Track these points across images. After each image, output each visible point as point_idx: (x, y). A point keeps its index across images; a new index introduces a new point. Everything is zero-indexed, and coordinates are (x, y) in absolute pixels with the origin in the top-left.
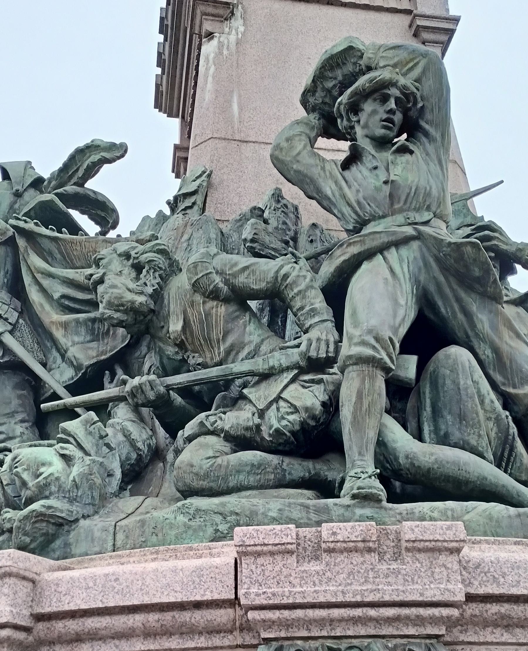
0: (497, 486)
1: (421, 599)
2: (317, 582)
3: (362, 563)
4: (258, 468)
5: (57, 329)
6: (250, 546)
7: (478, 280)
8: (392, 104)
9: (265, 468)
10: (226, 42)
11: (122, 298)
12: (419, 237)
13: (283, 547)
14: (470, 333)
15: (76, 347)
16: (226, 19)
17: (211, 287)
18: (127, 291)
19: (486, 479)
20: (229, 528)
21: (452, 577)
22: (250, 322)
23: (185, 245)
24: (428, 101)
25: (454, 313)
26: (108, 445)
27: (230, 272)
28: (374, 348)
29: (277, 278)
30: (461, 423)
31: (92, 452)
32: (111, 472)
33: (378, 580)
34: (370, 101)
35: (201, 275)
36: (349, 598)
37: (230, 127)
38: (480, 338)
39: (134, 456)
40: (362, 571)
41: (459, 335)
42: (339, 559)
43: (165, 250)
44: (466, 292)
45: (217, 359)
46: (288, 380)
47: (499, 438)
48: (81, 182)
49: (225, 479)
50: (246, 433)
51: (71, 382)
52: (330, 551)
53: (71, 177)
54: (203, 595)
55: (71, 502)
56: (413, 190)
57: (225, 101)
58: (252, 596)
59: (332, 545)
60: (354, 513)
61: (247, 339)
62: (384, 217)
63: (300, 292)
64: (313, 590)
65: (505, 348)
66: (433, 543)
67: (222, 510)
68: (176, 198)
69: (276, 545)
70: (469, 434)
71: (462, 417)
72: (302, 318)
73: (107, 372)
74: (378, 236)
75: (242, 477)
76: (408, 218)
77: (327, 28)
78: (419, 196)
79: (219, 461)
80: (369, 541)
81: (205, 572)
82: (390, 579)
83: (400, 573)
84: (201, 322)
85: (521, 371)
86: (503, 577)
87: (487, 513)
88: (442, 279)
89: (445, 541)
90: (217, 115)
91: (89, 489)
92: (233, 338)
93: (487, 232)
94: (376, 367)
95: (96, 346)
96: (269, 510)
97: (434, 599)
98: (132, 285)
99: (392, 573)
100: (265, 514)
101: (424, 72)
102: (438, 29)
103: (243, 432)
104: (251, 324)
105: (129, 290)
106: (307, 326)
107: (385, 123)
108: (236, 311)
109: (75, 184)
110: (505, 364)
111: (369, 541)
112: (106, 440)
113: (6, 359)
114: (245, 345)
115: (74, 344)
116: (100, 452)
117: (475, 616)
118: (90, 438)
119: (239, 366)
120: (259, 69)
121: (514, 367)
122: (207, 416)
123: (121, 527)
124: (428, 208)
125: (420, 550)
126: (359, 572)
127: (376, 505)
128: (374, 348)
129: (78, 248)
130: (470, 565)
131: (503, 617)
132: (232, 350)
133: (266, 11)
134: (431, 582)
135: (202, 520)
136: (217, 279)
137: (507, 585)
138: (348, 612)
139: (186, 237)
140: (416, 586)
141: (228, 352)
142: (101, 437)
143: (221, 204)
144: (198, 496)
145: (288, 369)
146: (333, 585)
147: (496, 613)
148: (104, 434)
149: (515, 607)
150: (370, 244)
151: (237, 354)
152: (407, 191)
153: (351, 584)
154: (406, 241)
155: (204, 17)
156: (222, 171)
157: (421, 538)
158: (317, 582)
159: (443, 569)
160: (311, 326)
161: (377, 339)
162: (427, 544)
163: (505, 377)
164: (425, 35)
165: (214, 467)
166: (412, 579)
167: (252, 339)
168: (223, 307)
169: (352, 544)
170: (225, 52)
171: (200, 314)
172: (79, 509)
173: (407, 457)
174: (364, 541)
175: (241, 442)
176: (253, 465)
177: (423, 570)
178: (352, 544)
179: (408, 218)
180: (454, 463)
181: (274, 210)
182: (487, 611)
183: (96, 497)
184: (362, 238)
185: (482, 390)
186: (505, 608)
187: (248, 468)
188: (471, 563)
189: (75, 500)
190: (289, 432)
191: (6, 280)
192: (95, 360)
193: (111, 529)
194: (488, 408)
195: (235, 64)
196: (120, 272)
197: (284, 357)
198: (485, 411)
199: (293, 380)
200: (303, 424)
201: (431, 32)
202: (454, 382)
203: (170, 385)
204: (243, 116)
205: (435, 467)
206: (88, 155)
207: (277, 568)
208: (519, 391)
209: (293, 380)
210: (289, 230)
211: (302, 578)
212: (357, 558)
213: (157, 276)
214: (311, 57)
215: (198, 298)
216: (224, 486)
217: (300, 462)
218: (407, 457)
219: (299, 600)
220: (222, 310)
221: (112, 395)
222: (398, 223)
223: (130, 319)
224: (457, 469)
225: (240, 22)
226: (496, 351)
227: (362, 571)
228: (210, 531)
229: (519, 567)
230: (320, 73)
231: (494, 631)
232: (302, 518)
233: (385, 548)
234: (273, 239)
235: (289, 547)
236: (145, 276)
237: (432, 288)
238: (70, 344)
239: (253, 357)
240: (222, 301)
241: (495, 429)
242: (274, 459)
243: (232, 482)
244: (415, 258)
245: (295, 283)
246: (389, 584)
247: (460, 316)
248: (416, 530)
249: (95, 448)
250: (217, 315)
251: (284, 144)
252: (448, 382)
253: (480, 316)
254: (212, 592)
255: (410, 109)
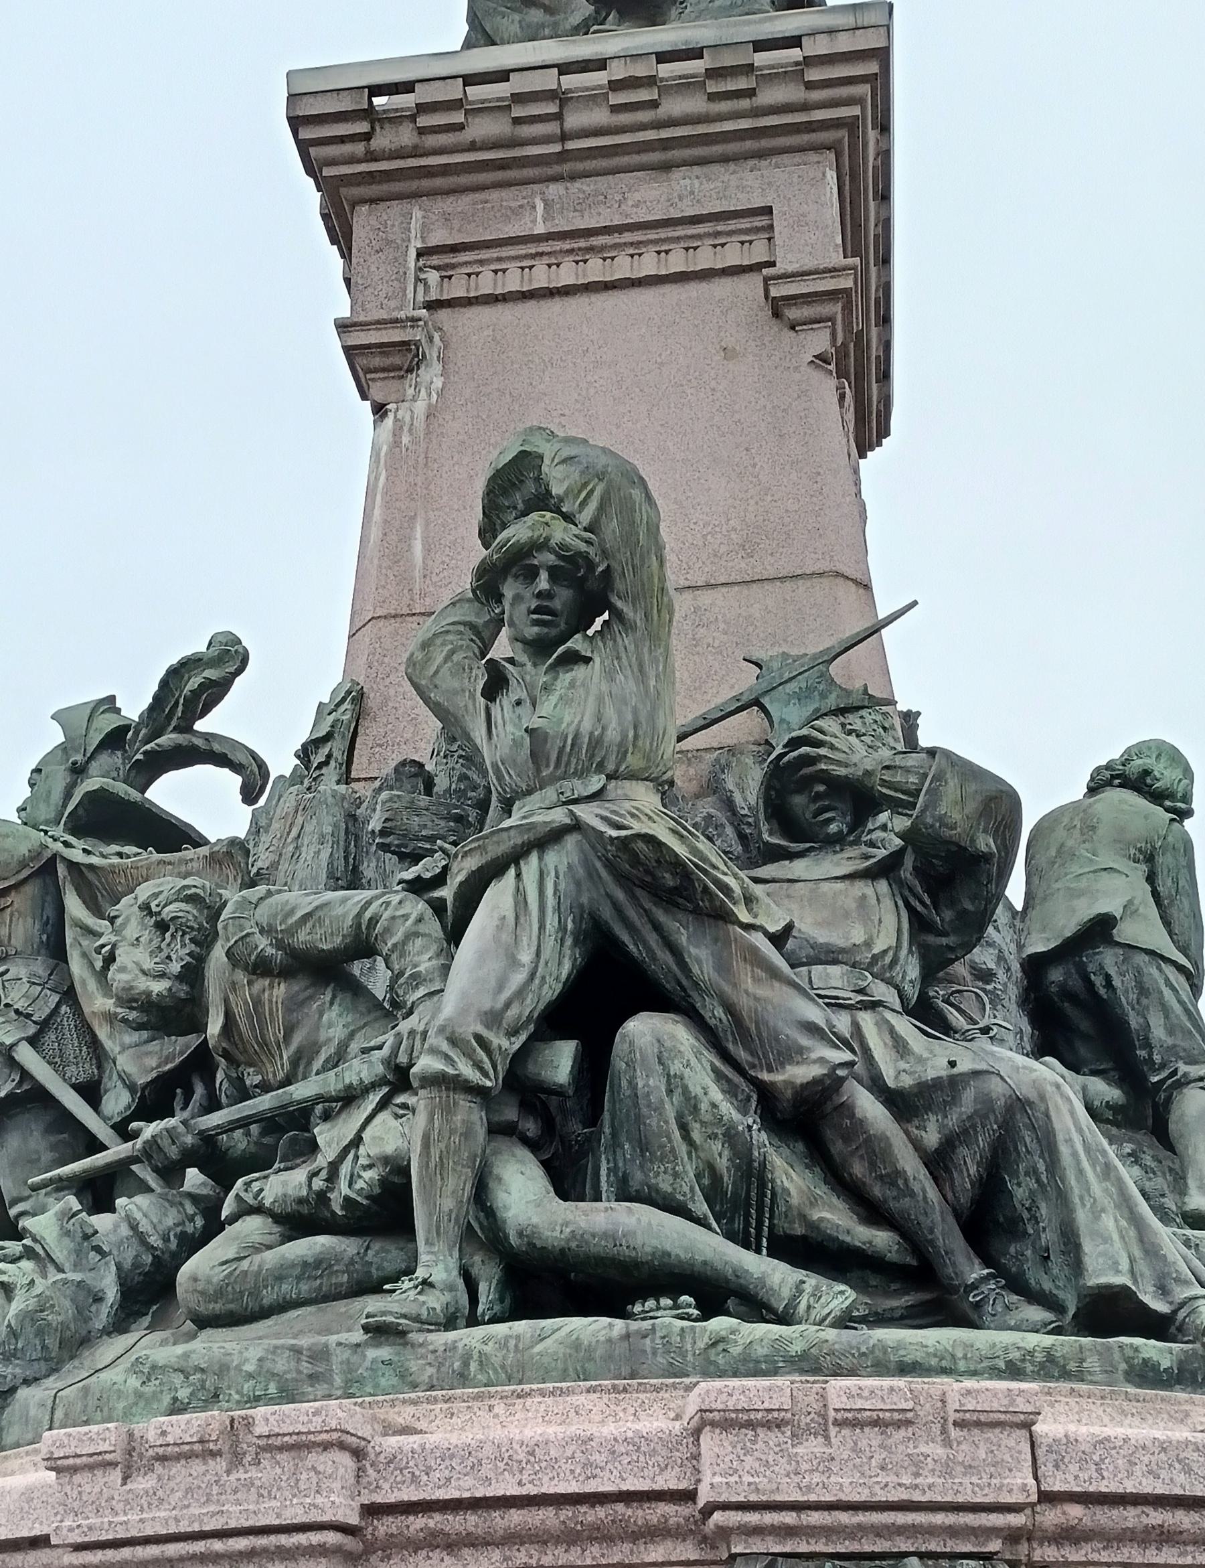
0: (693, 1265)
1: (277, 1522)
2: (145, 1506)
3: (204, 1474)
4: (317, 1267)
5: (100, 1025)
6: (60, 1458)
7: (676, 891)
8: (543, 583)
9: (331, 1266)
10: (407, 419)
11: (131, 988)
12: (576, 826)
13: (100, 1458)
14: (685, 982)
15: (128, 1052)
16: (410, 370)
17: (253, 957)
18: (140, 975)
19: (669, 1255)
20: (191, 1394)
21: (324, 1486)
22: (332, 1004)
23: (291, 848)
24: (614, 557)
25: (649, 950)
26: (98, 1249)
27: (283, 927)
28: (447, 1057)
29: (360, 924)
30: (643, 1156)
31: (67, 1267)
32: (100, 1294)
33: (223, 1497)
34: (510, 580)
35: (232, 942)
36: (184, 1527)
37: (405, 591)
38: (701, 989)
39: (148, 1259)
40: (204, 1486)
41: (668, 986)
42: (174, 1471)
43: (197, 895)
44: (666, 911)
45: (281, 1075)
46: (373, 1106)
47: (738, 1168)
48: (183, 724)
49: (255, 1293)
50: (300, 1208)
51: (128, 1113)
52: (163, 1459)
53: (169, 717)
54: (31, 1529)
55: (8, 1360)
56: (569, 741)
57: (400, 541)
58: (65, 1531)
59: (161, 1451)
60: (365, 1356)
61: (323, 1035)
62: (529, 792)
63: (395, 945)
64: (138, 1518)
65: (744, 1003)
66: (295, 1437)
67: (185, 1364)
68: (305, 747)
69: (91, 1455)
70: (657, 1174)
71: (643, 1146)
72: (401, 992)
73: (178, 1091)
74: (505, 835)
75: (285, 1287)
76: (562, 793)
77: (601, 342)
78: (580, 748)
79: (245, 1265)
80: (208, 1441)
81: (35, 1495)
82: (239, 1495)
83: (253, 1484)
84: (249, 1016)
85: (777, 1040)
86: (427, 1474)
87: (574, 1337)
88: (620, 895)
89: (310, 1433)
90: (384, 571)
91: (36, 1336)
92: (300, 1039)
93: (804, 750)
94: (454, 1089)
95: (158, 1048)
96: (247, 1360)
97: (295, 1521)
98: (148, 964)
99: (243, 1486)
100: (238, 1368)
101: (601, 508)
102: (816, 294)
103: (295, 1207)
104: (335, 1007)
105: (144, 972)
106: (409, 1004)
107: (535, 616)
108: (306, 988)
109: (175, 729)
110: (748, 1030)
111: (208, 1441)
112: (95, 1241)
113: (26, 1087)
114: (321, 1047)
115: (124, 1048)
116: (84, 1261)
117: (392, 1535)
118: (66, 1241)
119: (301, 1091)
120: (466, 460)
121: (765, 1035)
122: (248, 1184)
123: (62, 1397)
124: (600, 768)
125: (281, 1449)
126: (199, 1487)
127: (399, 1341)
128: (447, 1057)
129: (123, 881)
130: (382, 1458)
131: (434, 1534)
132: (299, 1059)
133: (486, 333)
134: (294, 1496)
135: (157, 1382)
136: (263, 943)
137: (432, 1485)
138: (187, 1548)
139: (294, 833)
140: (274, 1503)
141: (295, 1062)
142: (86, 1237)
143: (381, 746)
144: (211, 1327)
145: (373, 1086)
146: (165, 1510)
147: (422, 1529)
148: (90, 1231)
149: (450, 1518)
150: (497, 849)
151: (309, 1063)
152: (559, 743)
153: (188, 1506)
154: (554, 836)
155: (368, 376)
156: (387, 681)
157: (277, 1430)
158: (145, 1506)
159: (312, 1474)
160: (413, 1003)
161: (453, 1041)
162: (286, 1439)
163: (753, 1053)
164: (793, 313)
165: (232, 1279)
166: (269, 1492)
167: (331, 1035)
168: (282, 985)
169: (187, 1447)
170: (405, 439)
171: (246, 1003)
172: (18, 1370)
173: (520, 1234)
174: (201, 1442)
175: (297, 1221)
176: (305, 1264)
177: (284, 1478)
178: (187, 1447)
179: (562, 793)
180: (605, 1235)
181: (445, 757)
182: (408, 1527)
183: (51, 1346)
184: (481, 843)
185: (691, 1088)
186: (434, 1521)
187: (297, 1271)
188: (382, 1455)
189: (14, 1355)
190: (367, 1198)
191: (44, 937)
192: (154, 1074)
193: (49, 1403)
194: (707, 1117)
195: (421, 460)
196: (137, 939)
197: (366, 1066)
198: (703, 1124)
199: (383, 1105)
200: (383, 1182)
201: (804, 303)
202: (630, 1082)
203: (204, 1131)
204: (430, 563)
205: (573, 1245)
206: (186, 676)
207: (97, 1489)
208: (777, 1078)
209: (383, 1105)
210: (474, 789)
211: (127, 1502)
212: (197, 1467)
213: (187, 941)
214: (567, 412)
215: (241, 977)
216: (252, 1305)
217: (402, 1245)
218: (520, 1234)
219: (122, 1534)
220: (281, 990)
221: (123, 1156)
222: (547, 803)
223: (153, 1020)
224: (611, 1245)
225: (437, 367)
226: (730, 1008)
227: (204, 1486)
228: (166, 1399)
229: (452, 1457)
230: (489, 501)
231: (431, 1554)
232: (288, 1372)
233: (245, 1446)
234: (426, 819)
235: (108, 1457)
236: (169, 945)
237: (607, 913)
238: (117, 1049)
239: (336, 1066)
240: (279, 975)
241: (726, 1153)
242: (346, 1246)
243: (269, 1296)
244: (570, 866)
245: (387, 930)
246: (238, 1503)
247: (665, 957)
248: (271, 1419)
249: (73, 1257)
250: (270, 1001)
251: (419, 656)
252: (624, 1083)
253: (693, 950)
254: (41, 1523)
255: (584, 579)
